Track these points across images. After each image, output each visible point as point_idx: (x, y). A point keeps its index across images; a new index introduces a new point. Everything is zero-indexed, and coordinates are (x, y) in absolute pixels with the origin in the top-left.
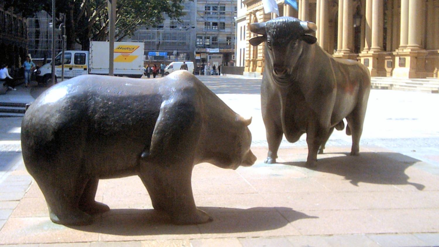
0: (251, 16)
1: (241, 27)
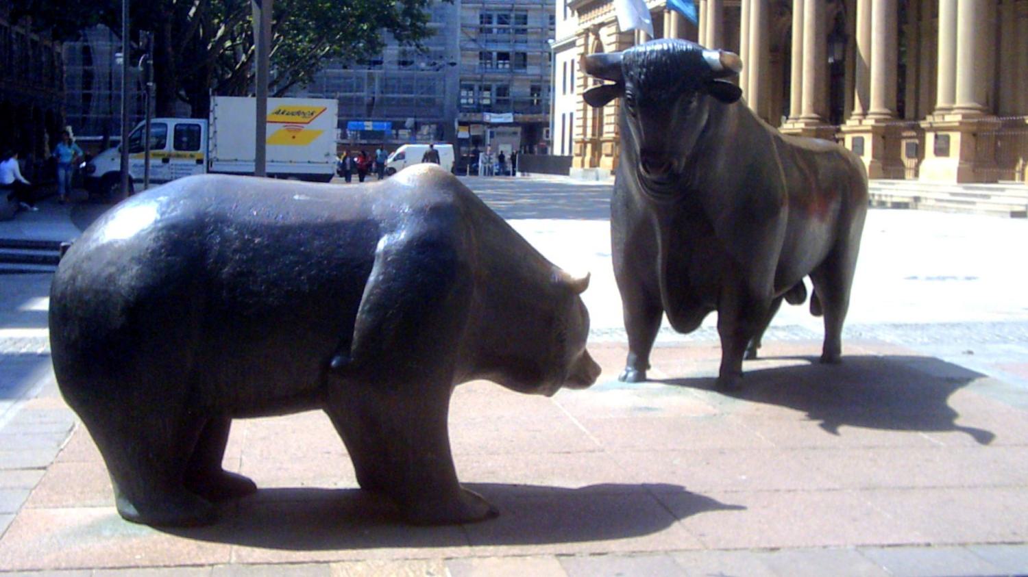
1: (565, 64)
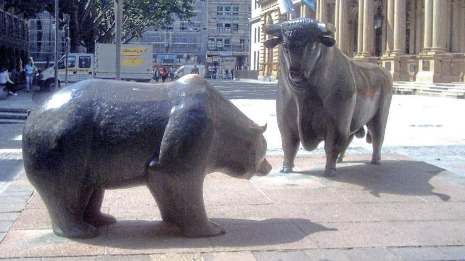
0: (266, 17)
